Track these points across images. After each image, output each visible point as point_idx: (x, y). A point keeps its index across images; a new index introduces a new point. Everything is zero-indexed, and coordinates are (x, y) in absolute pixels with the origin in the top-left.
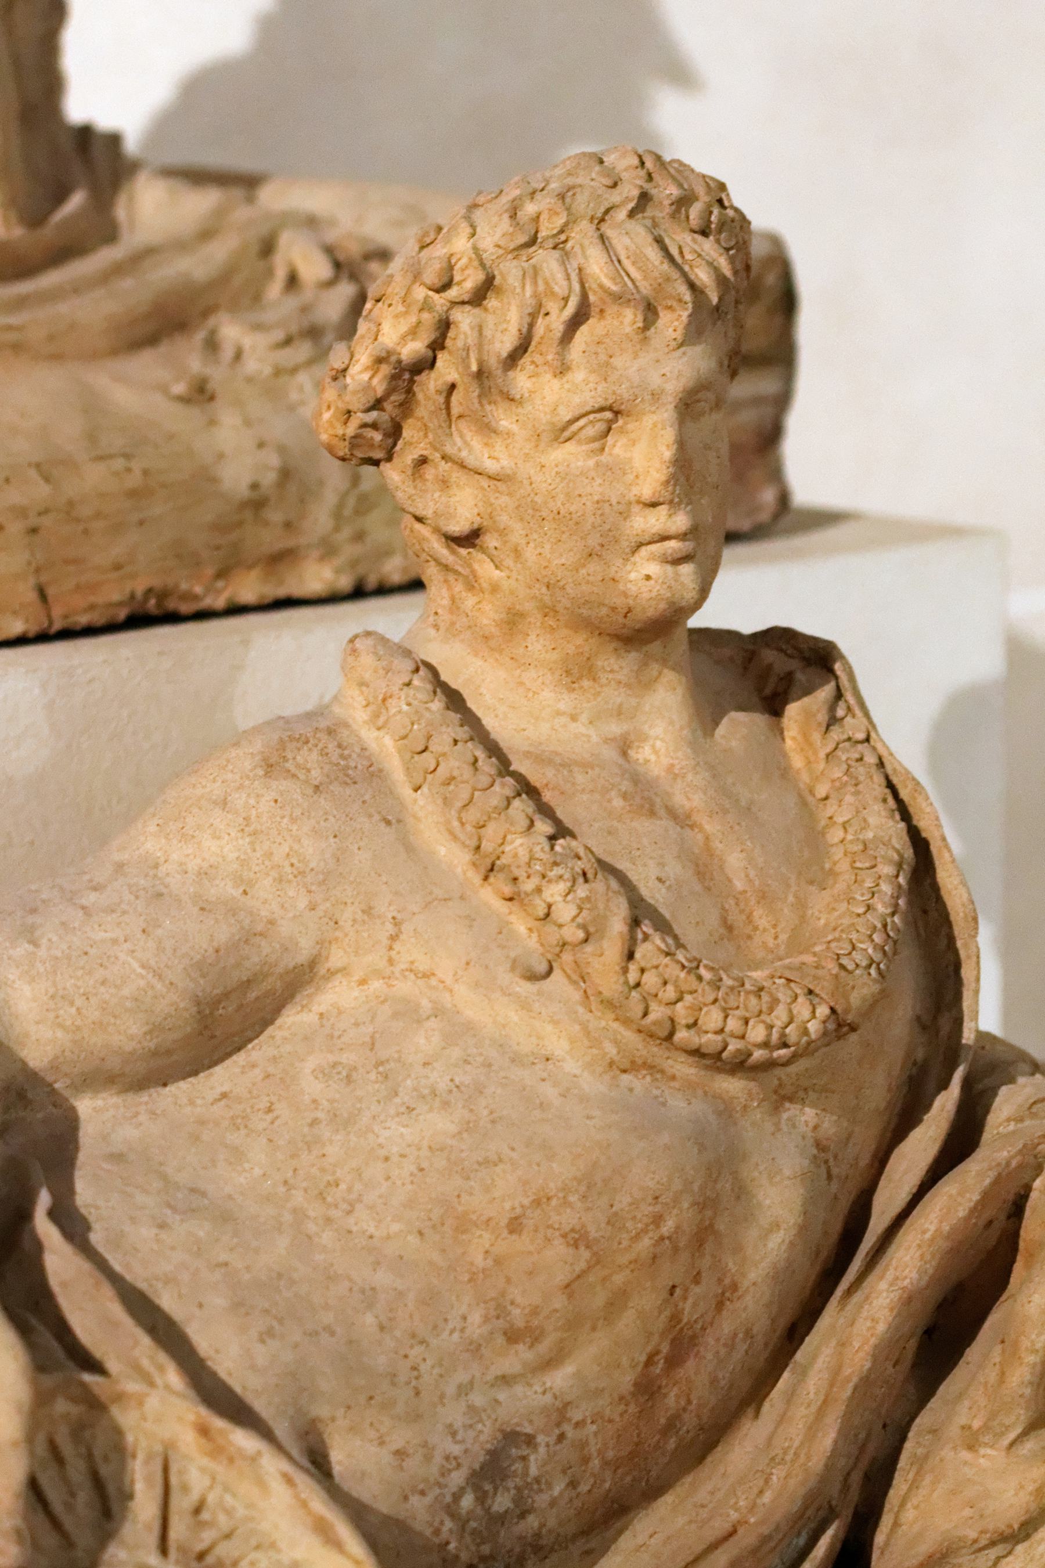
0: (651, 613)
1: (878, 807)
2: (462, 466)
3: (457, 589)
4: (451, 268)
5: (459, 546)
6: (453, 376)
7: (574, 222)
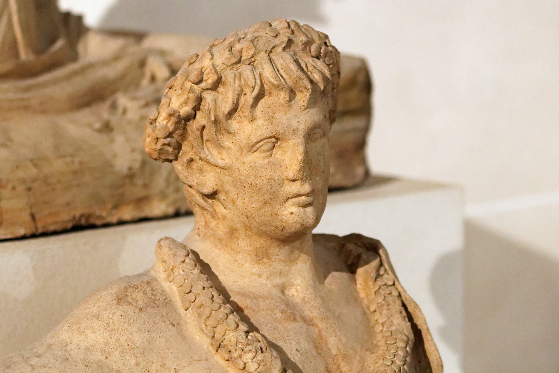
0: (293, 229)
1: (398, 315)
2: (208, 162)
3: (208, 218)
4: (202, 73)
5: (209, 198)
6: (203, 122)
7: (258, 53)
